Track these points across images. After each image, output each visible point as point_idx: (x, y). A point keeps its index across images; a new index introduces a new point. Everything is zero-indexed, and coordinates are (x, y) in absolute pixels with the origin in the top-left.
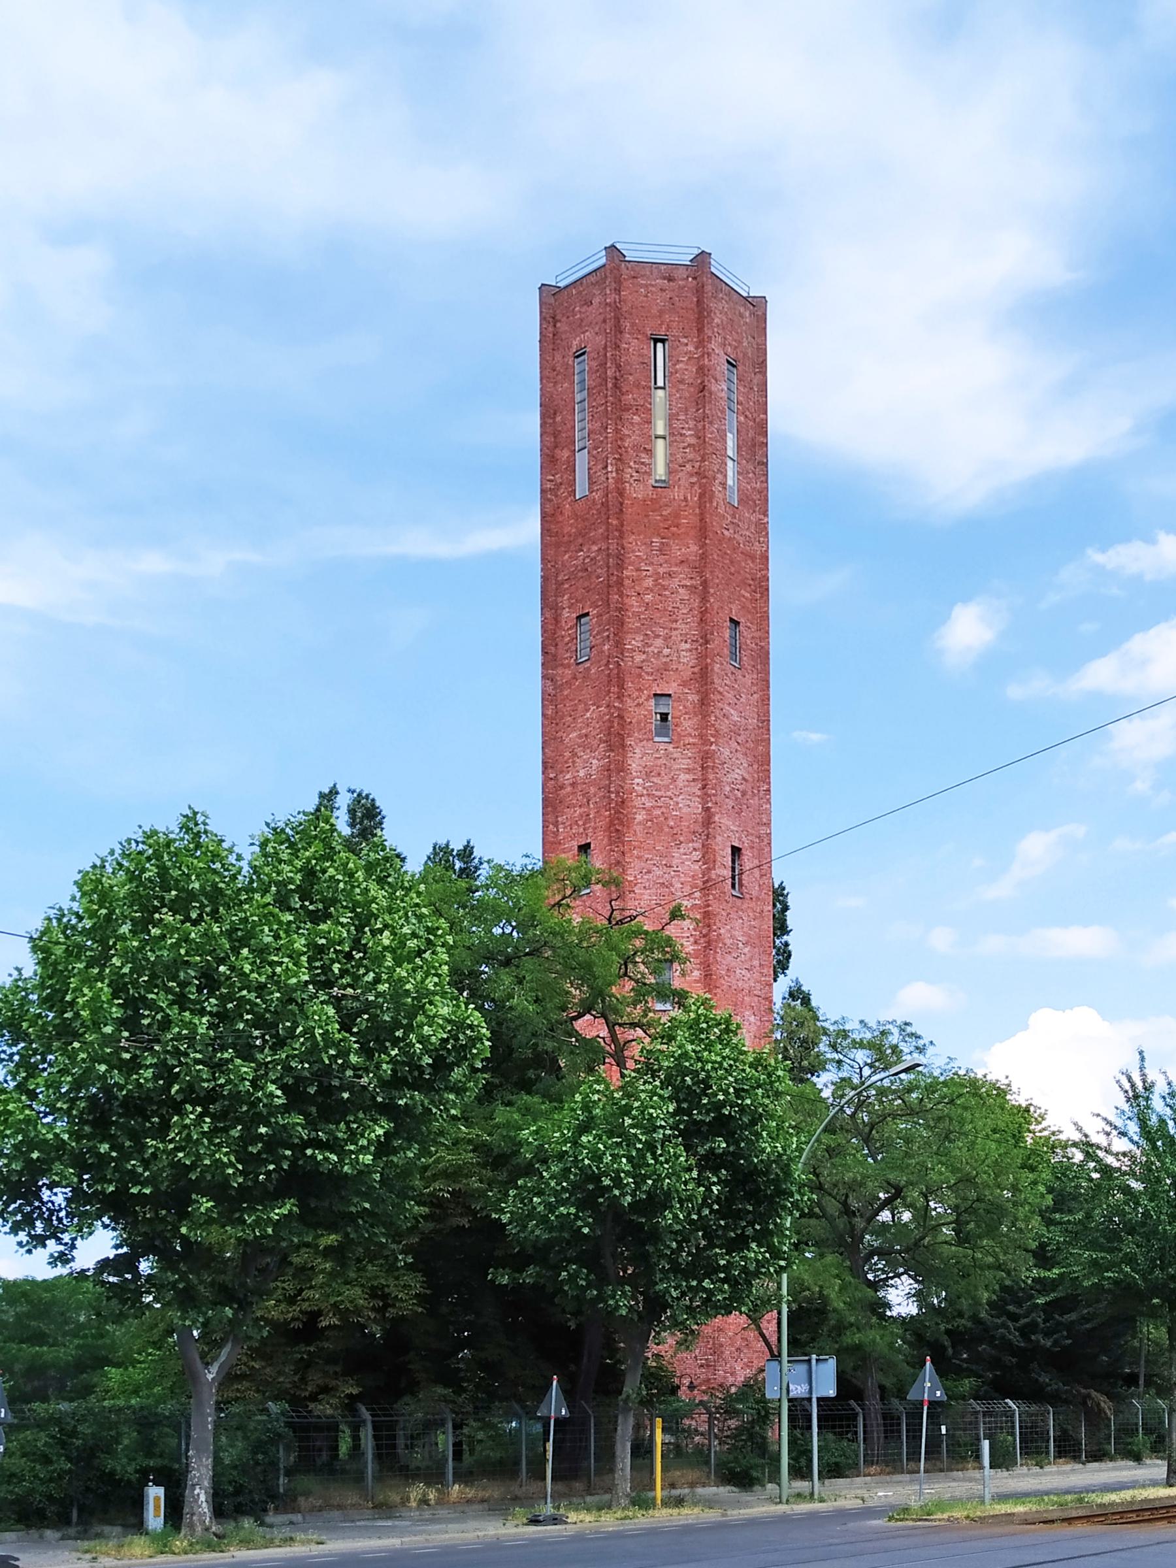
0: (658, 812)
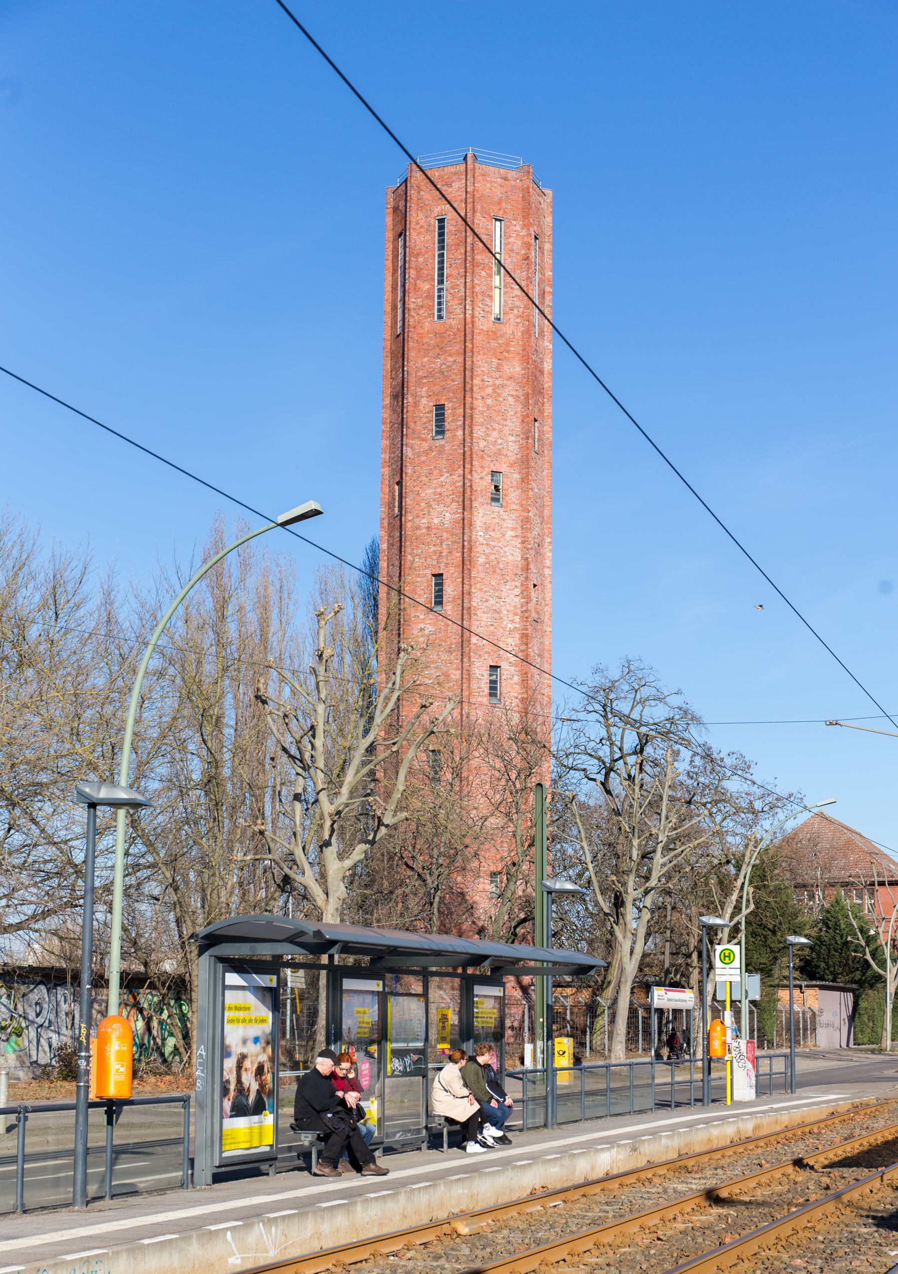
0: (492, 557)
